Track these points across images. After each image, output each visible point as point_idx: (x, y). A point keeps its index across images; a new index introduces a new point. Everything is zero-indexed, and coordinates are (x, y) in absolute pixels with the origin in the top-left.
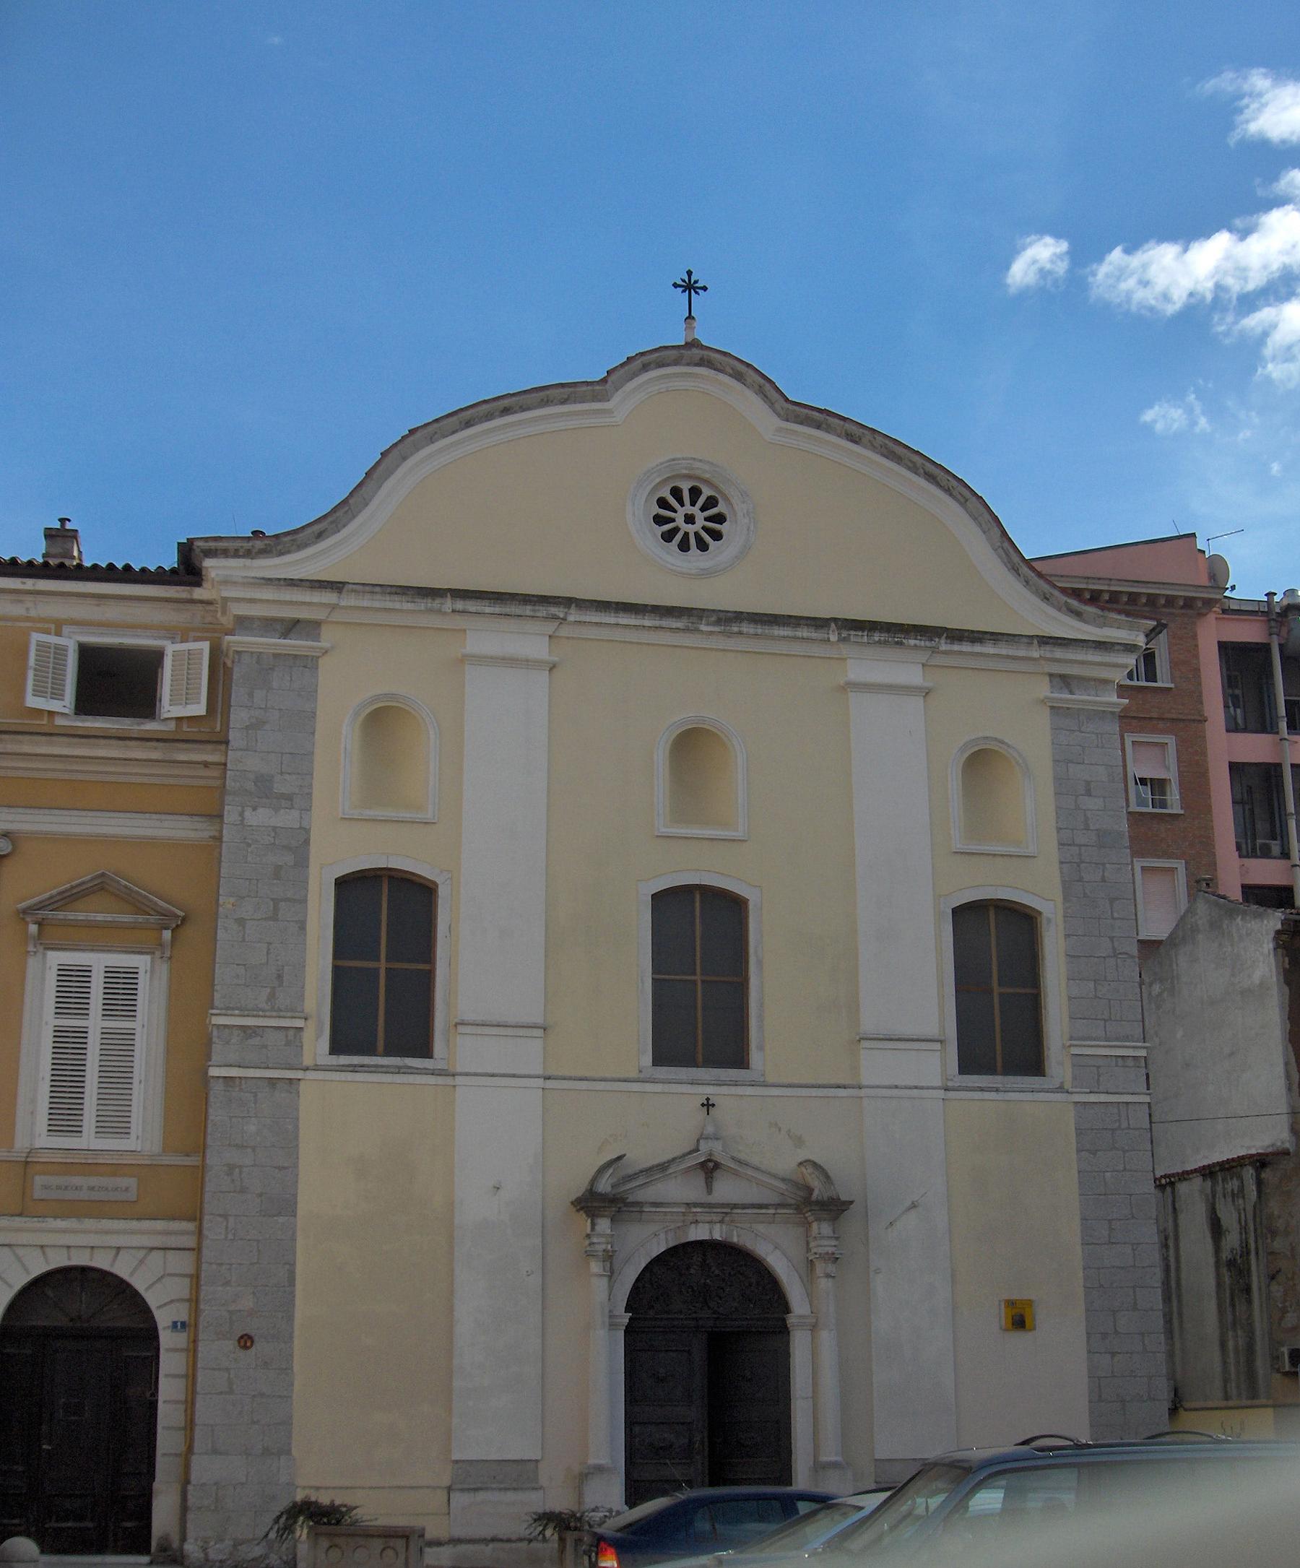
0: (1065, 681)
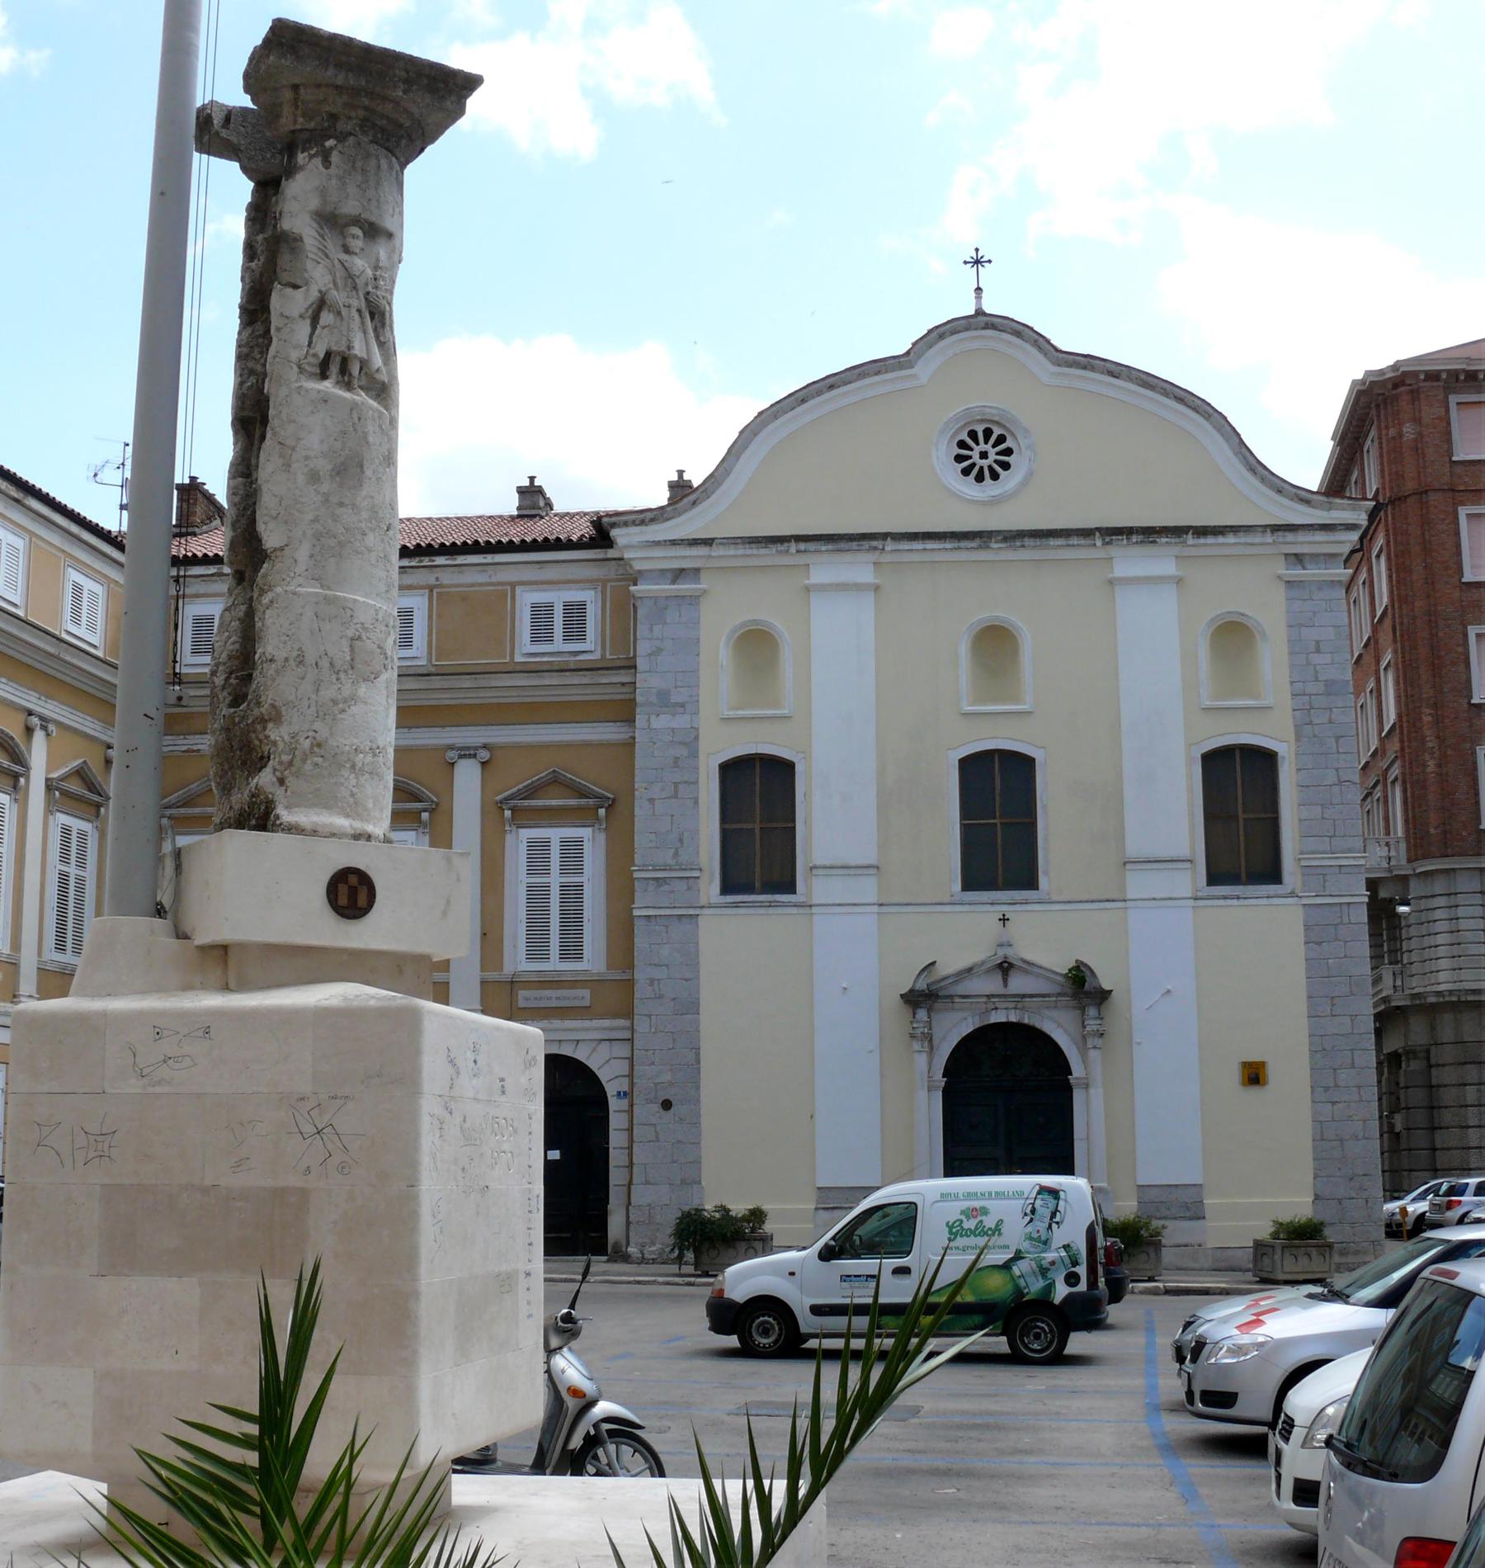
0: (1298, 559)
